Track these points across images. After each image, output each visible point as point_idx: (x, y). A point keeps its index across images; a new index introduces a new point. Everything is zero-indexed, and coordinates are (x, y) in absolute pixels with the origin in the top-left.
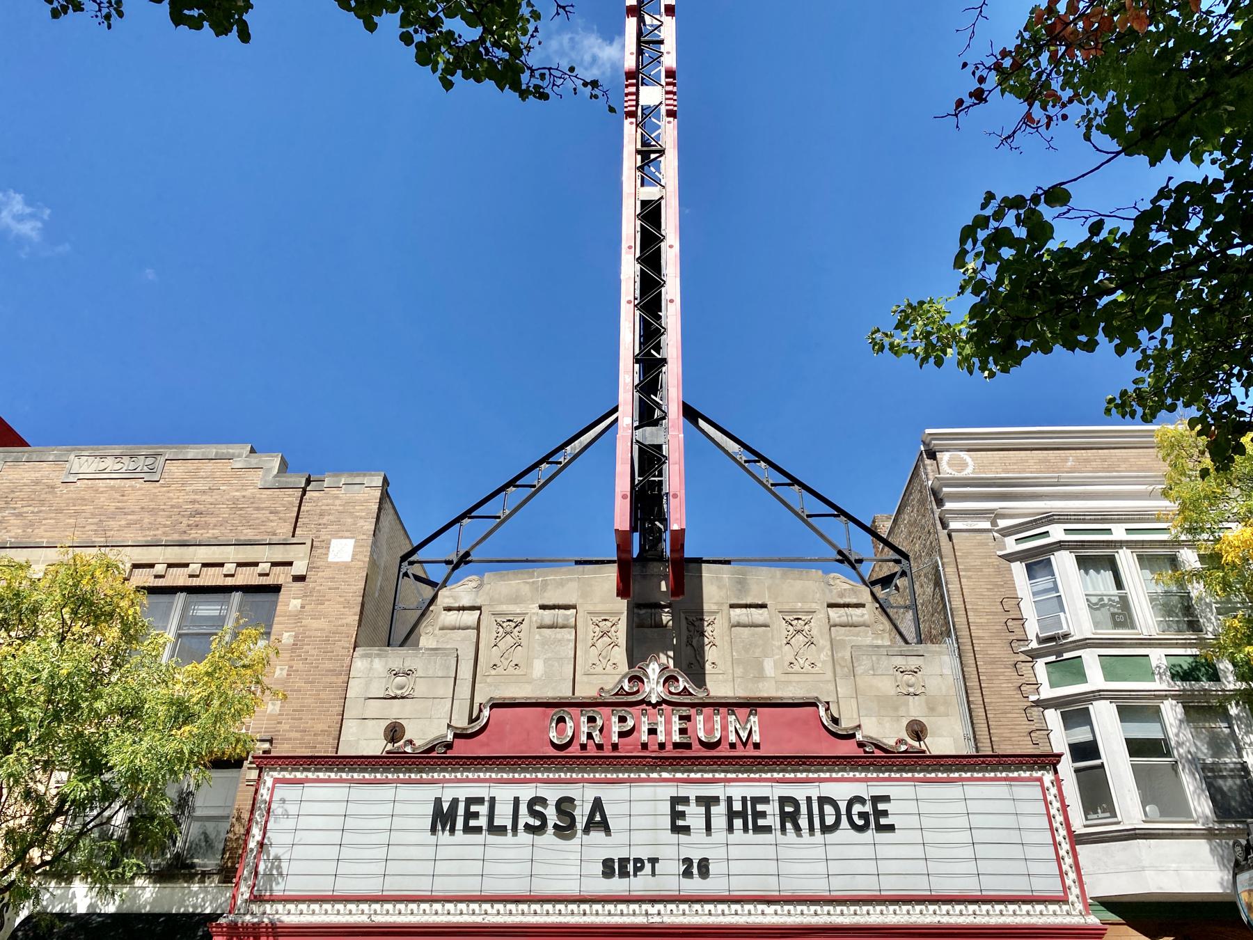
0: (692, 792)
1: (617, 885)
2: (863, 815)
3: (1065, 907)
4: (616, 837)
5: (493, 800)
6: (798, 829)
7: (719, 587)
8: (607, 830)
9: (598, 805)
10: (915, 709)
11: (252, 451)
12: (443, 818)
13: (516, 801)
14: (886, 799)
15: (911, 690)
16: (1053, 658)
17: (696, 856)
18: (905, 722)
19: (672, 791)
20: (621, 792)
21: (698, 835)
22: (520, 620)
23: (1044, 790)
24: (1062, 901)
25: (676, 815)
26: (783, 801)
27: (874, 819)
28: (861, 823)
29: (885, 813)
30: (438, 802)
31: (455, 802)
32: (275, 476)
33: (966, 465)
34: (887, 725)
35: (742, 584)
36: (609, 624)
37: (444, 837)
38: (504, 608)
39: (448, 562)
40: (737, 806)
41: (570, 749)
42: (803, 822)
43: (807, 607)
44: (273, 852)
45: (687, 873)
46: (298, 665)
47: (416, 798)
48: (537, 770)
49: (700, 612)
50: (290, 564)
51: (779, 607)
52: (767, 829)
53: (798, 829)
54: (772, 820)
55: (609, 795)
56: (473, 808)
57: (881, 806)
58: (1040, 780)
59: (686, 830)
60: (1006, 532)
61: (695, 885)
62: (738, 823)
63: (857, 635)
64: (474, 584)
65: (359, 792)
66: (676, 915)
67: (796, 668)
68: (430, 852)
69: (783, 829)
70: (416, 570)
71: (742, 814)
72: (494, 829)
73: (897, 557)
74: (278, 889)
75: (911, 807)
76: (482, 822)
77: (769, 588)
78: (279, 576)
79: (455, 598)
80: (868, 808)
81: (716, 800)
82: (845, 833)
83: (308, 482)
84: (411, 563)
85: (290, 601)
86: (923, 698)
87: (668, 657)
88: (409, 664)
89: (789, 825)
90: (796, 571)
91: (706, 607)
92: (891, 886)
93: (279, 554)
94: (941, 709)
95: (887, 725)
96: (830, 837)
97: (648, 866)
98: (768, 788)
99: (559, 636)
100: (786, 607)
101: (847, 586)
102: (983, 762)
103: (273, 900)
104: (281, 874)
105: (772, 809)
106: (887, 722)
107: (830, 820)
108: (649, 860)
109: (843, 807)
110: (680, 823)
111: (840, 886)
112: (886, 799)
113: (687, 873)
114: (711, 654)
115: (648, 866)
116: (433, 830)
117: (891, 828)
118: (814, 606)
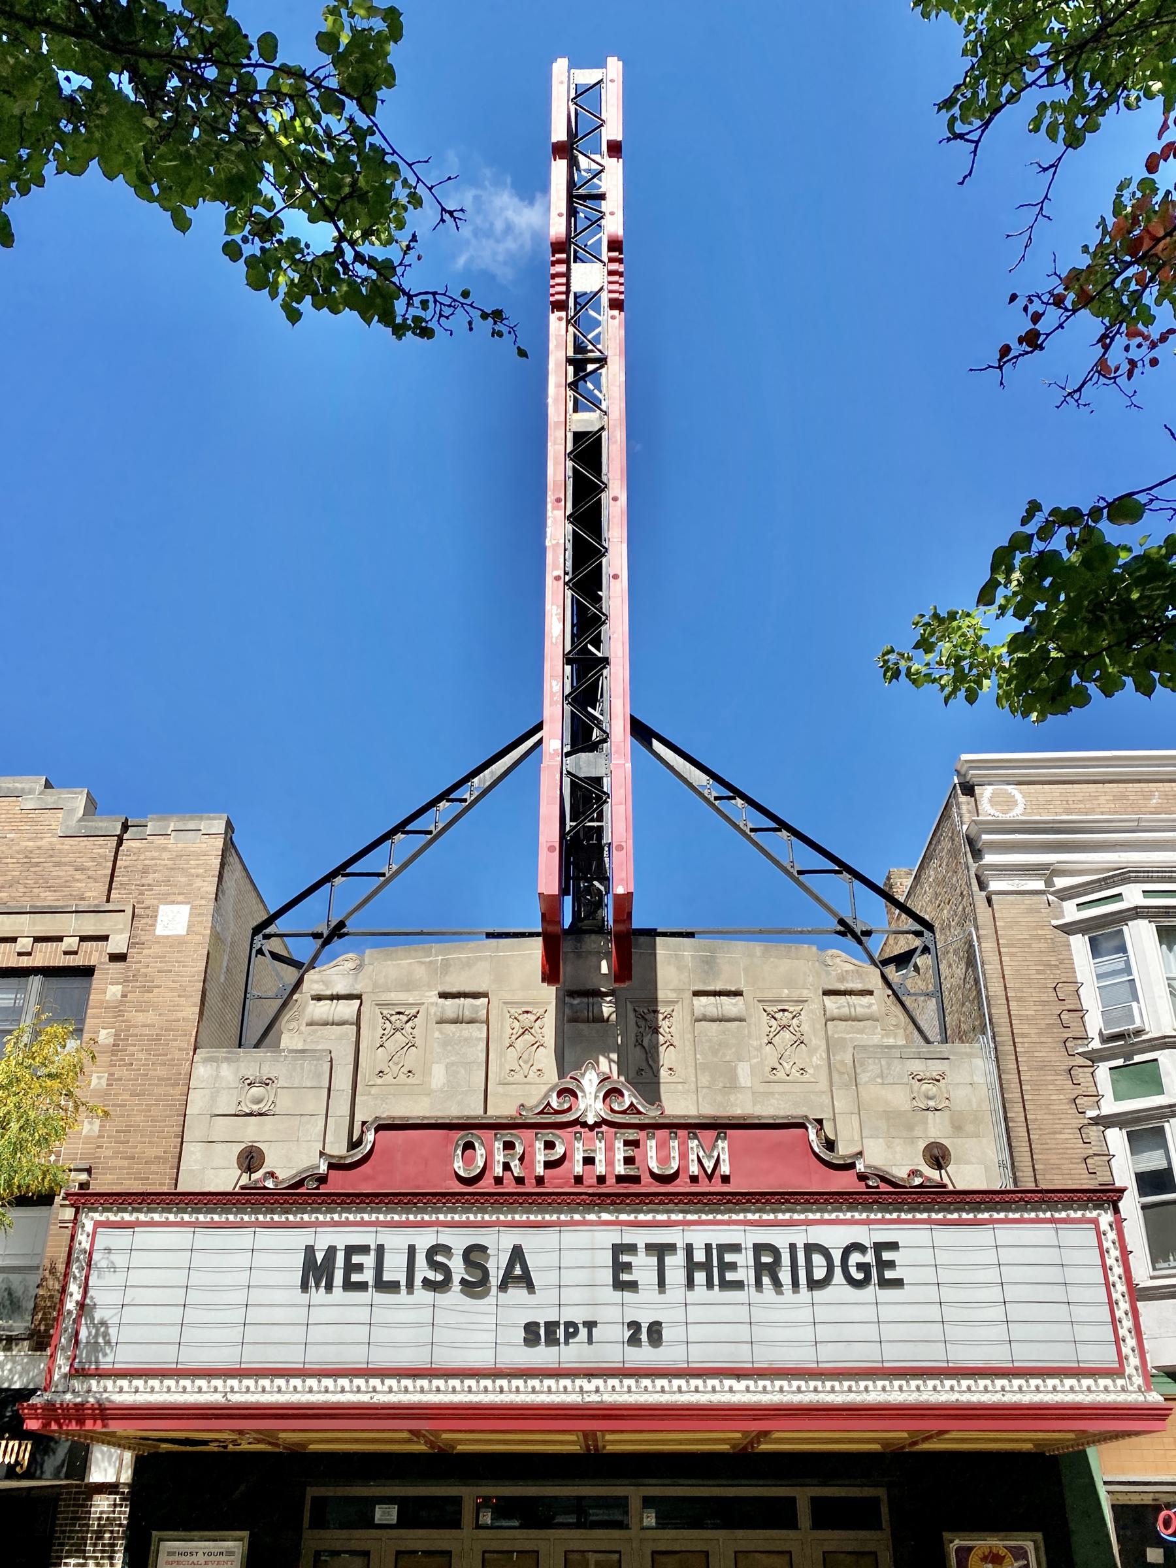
0: (641, 1237)
1: (543, 1356)
2: (860, 1267)
3: (1120, 1382)
4: (540, 1296)
5: (381, 1249)
6: (777, 1284)
7: (678, 968)
8: (530, 1287)
9: (517, 1254)
10: (936, 1129)
11: (48, 785)
12: (316, 1271)
13: (412, 1250)
14: (894, 1246)
15: (931, 1103)
16: (1120, 1062)
17: (645, 1319)
18: (922, 1145)
19: (614, 1237)
20: (548, 1238)
21: (648, 1292)
22: (413, 1012)
23: (1100, 1235)
24: (1116, 1372)
25: (620, 1267)
26: (759, 1249)
27: (876, 1271)
28: (859, 1276)
29: (891, 1264)
30: (310, 1251)
31: (331, 1251)
32: (80, 820)
33: (1015, 803)
34: (898, 1149)
35: (709, 964)
36: (532, 1017)
37: (318, 1295)
38: (394, 996)
39: (316, 936)
40: (699, 1256)
41: (481, 1183)
42: (785, 1276)
43: (795, 995)
44: (98, 1315)
45: (634, 1341)
46: (121, 1072)
47: (281, 1246)
48: (438, 1211)
49: (654, 1001)
50: (105, 938)
51: (760, 995)
52: (739, 1285)
53: (777, 1284)
54: (745, 1272)
55: (530, 1240)
56: (356, 1259)
57: (886, 1256)
58: (1095, 1221)
59: (633, 1286)
60: (1065, 894)
61: (645, 1355)
62: (700, 1277)
63: (861, 1032)
64: (350, 965)
65: (207, 1239)
66: (475, 1393)
67: (781, 1075)
68: (300, 1314)
69: (759, 1284)
70: (275, 945)
71: (706, 1266)
72: (385, 1286)
73: (918, 928)
74: (106, 1362)
75: (926, 1256)
76: (368, 1276)
77: (746, 970)
78: (91, 955)
79: (326, 984)
80: (869, 1258)
81: (672, 1248)
82: (839, 1289)
83: (125, 827)
84: (267, 937)
85: (107, 988)
86: (947, 1113)
87: (610, 1061)
88: (267, 1071)
89: (766, 1280)
90: (782, 947)
91: (661, 995)
92: (895, 1356)
93: (90, 925)
94: (970, 1128)
95: (898, 1149)
96: (819, 1295)
97: (583, 1332)
98: (742, 1232)
99: (465, 1034)
100: (769, 995)
101: (850, 967)
102: (1021, 1199)
103: (101, 1375)
104: (108, 1343)
105: (745, 1259)
106: (899, 1146)
107: (819, 1274)
108: (585, 1324)
109: (837, 1256)
110: (625, 1277)
111: (830, 1356)
112: (894, 1246)
113: (634, 1341)
114: (667, 1057)
115: (583, 1332)
116: (305, 1287)
117: (898, 1283)
118: (805, 993)
